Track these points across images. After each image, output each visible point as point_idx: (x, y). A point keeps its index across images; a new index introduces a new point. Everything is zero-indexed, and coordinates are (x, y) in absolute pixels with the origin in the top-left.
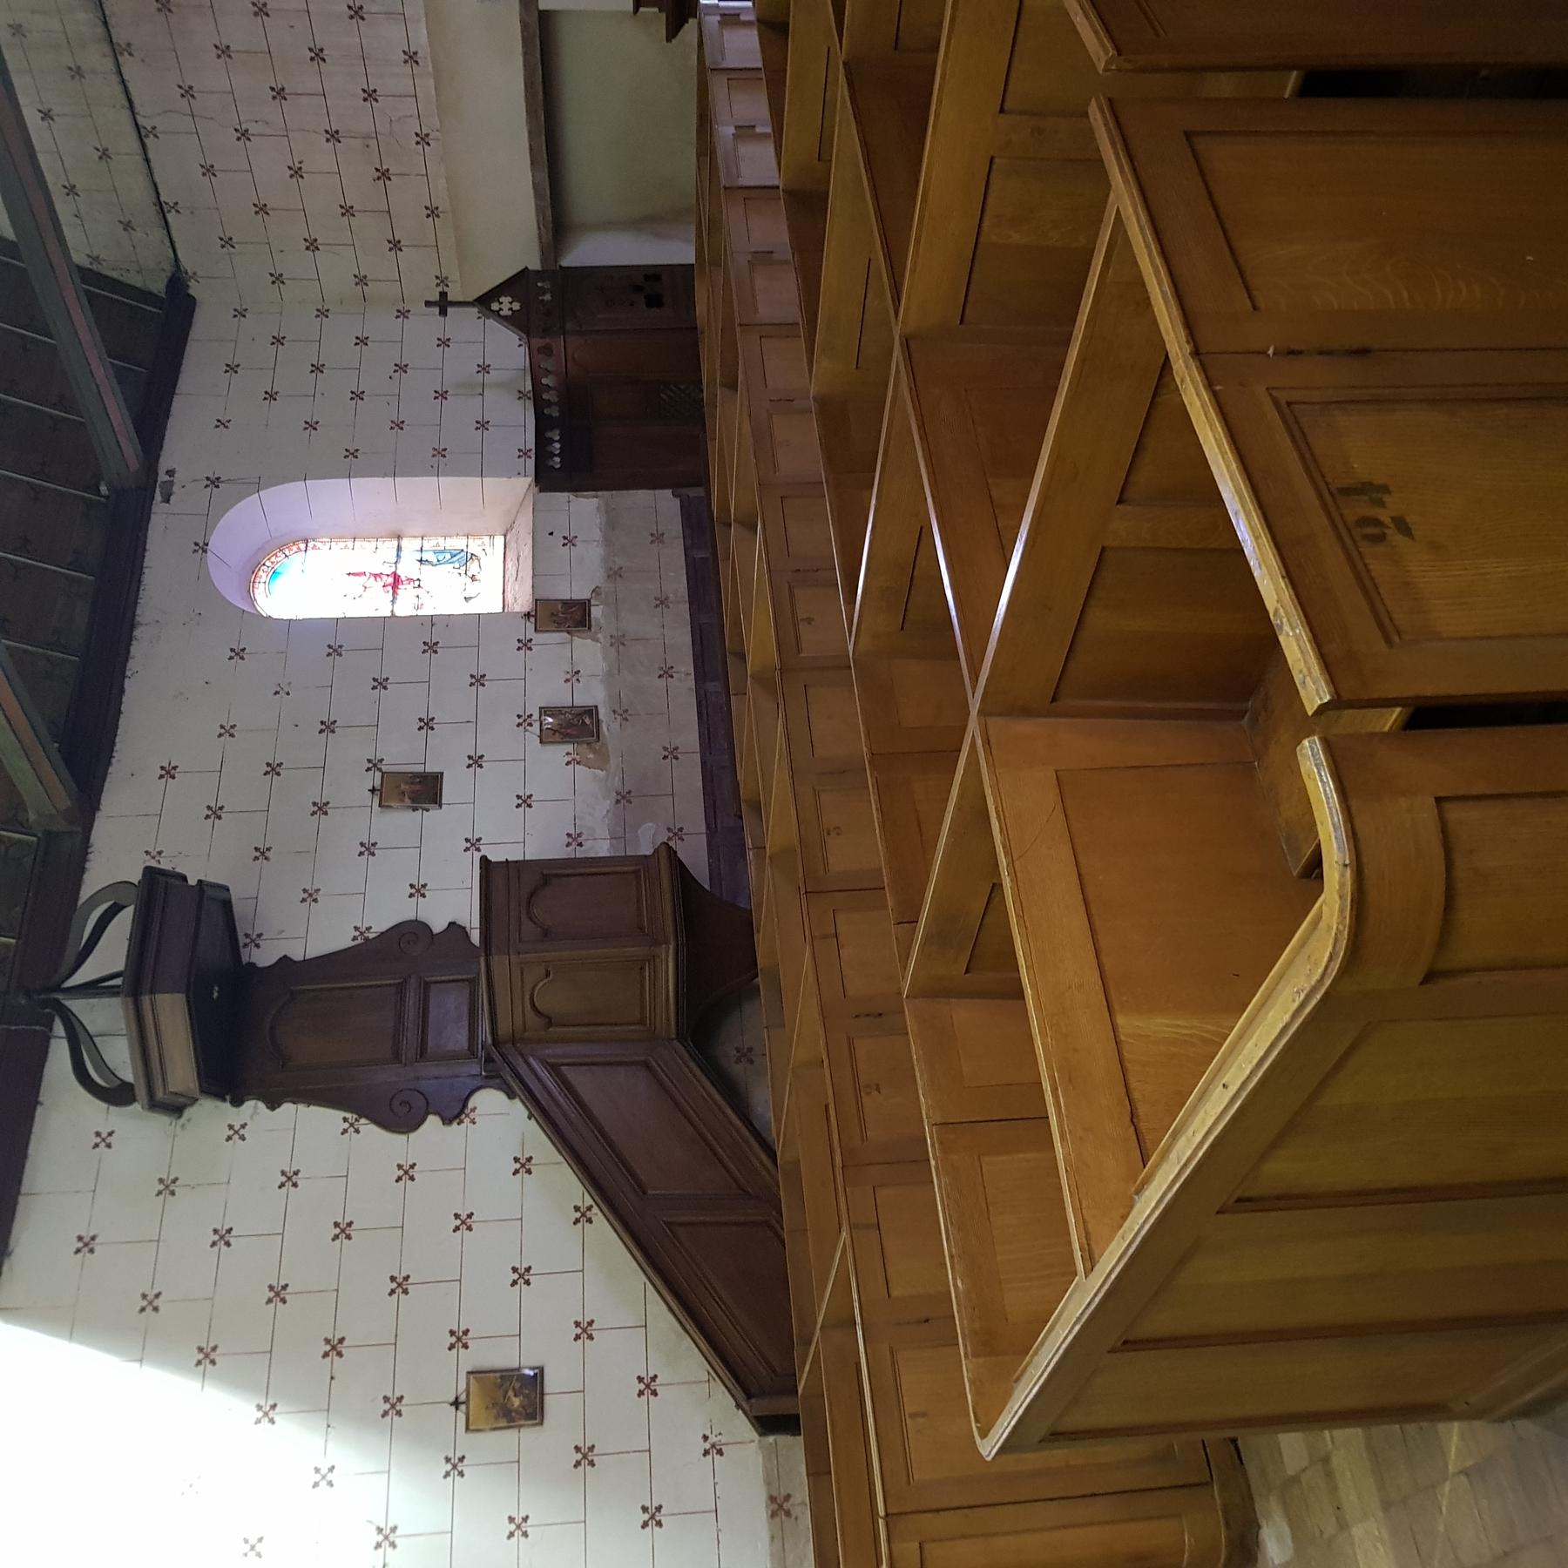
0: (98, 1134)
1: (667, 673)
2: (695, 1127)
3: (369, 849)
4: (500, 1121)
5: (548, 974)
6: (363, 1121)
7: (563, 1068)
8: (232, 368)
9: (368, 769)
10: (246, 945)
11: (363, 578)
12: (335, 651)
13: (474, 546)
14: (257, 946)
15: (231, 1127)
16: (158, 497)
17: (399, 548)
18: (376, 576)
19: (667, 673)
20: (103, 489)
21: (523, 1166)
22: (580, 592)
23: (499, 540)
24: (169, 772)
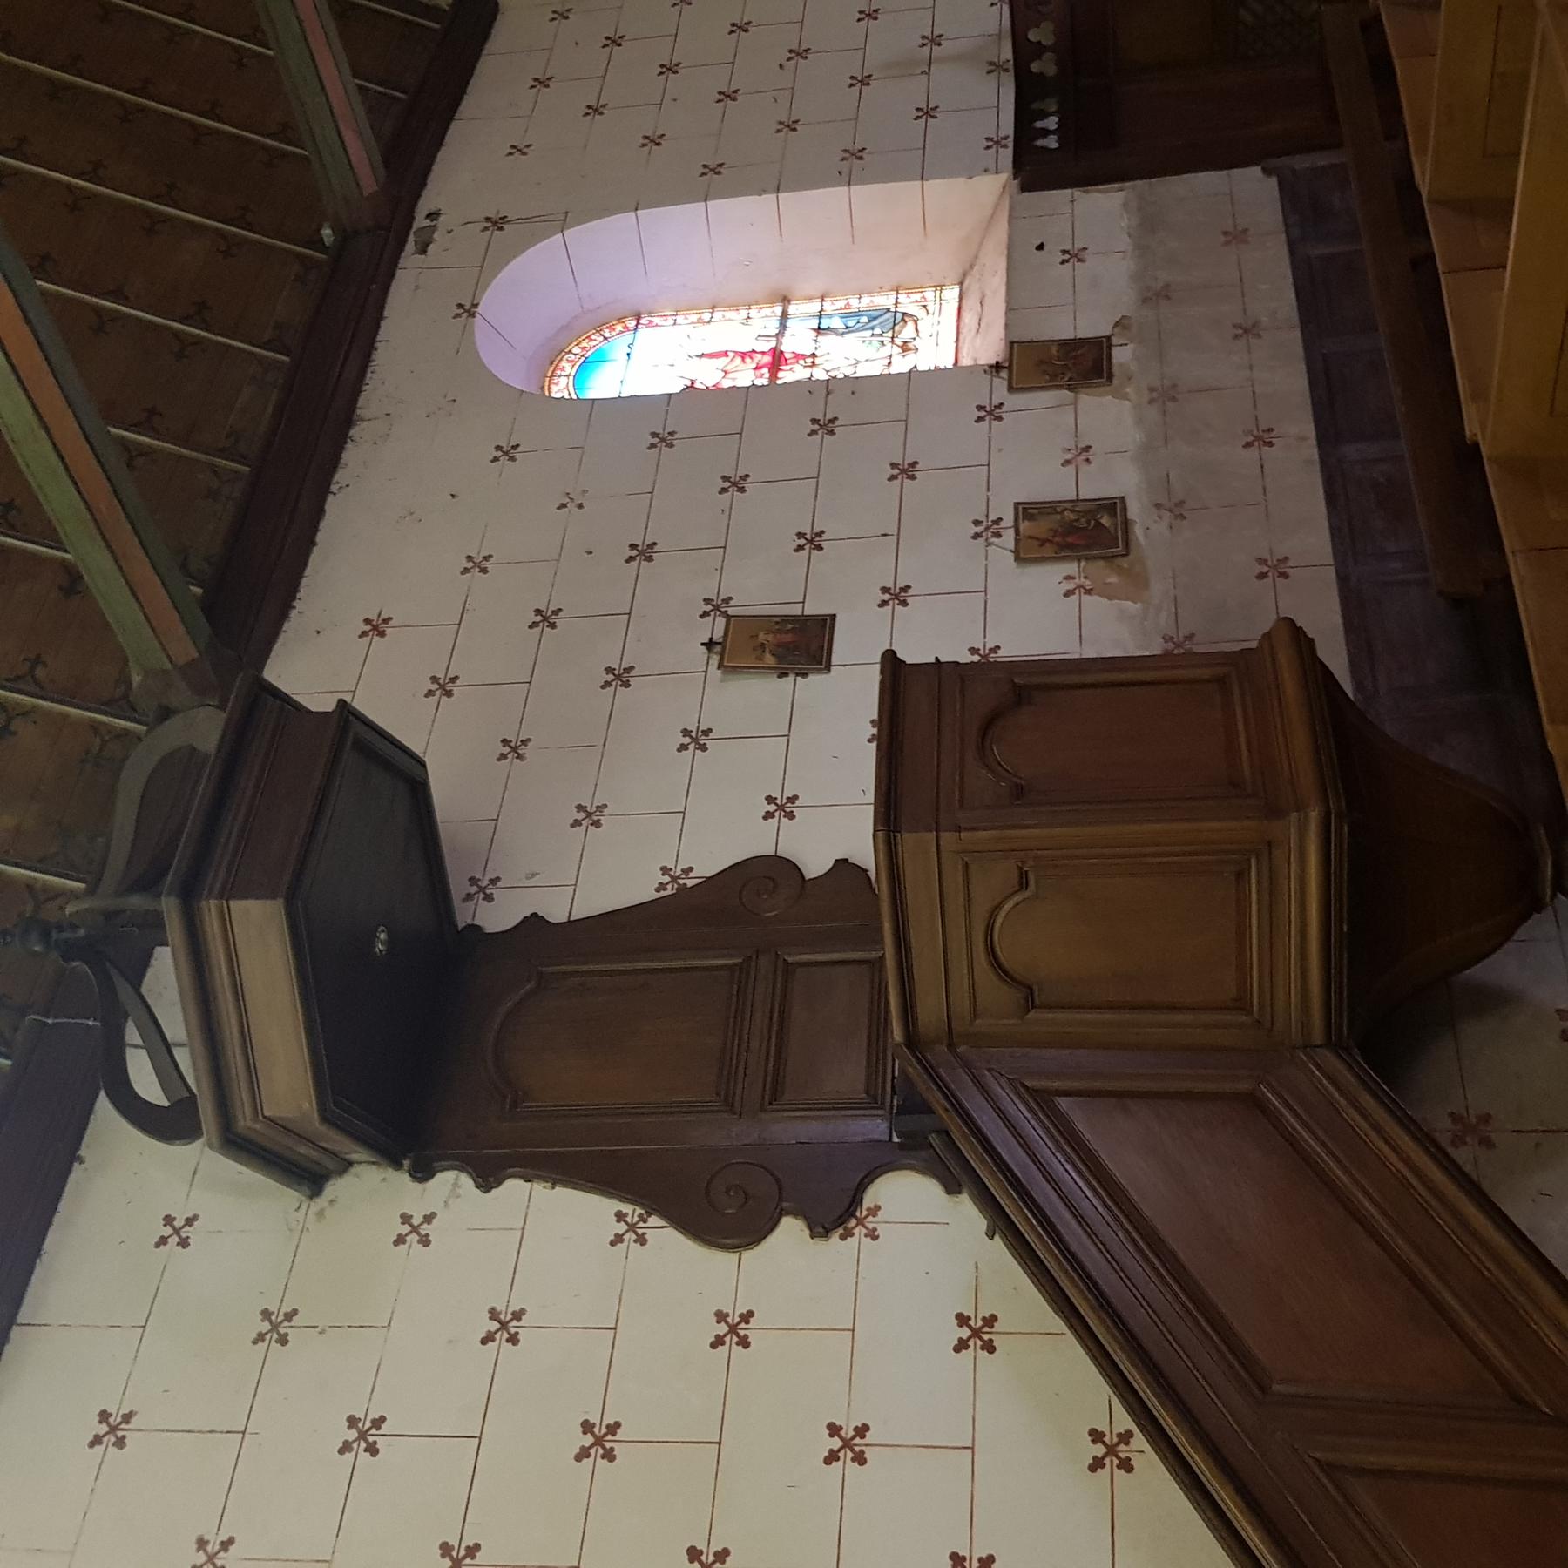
0: (168, 1220)
1: (1262, 439)
2: (1382, 1244)
3: (697, 739)
4: (924, 1232)
5: (1023, 883)
6: (654, 1220)
7: (1063, 1103)
8: (542, 82)
9: (705, 614)
10: (469, 897)
11: (723, 361)
12: (664, 440)
13: (908, 304)
14: (489, 898)
15: (406, 1219)
16: (410, 246)
17: (785, 316)
18: (743, 356)
19: (1262, 439)
20: (326, 232)
21: (976, 1333)
22: (1091, 325)
23: (952, 294)
24: (376, 627)
